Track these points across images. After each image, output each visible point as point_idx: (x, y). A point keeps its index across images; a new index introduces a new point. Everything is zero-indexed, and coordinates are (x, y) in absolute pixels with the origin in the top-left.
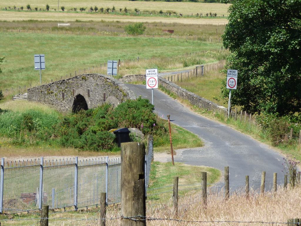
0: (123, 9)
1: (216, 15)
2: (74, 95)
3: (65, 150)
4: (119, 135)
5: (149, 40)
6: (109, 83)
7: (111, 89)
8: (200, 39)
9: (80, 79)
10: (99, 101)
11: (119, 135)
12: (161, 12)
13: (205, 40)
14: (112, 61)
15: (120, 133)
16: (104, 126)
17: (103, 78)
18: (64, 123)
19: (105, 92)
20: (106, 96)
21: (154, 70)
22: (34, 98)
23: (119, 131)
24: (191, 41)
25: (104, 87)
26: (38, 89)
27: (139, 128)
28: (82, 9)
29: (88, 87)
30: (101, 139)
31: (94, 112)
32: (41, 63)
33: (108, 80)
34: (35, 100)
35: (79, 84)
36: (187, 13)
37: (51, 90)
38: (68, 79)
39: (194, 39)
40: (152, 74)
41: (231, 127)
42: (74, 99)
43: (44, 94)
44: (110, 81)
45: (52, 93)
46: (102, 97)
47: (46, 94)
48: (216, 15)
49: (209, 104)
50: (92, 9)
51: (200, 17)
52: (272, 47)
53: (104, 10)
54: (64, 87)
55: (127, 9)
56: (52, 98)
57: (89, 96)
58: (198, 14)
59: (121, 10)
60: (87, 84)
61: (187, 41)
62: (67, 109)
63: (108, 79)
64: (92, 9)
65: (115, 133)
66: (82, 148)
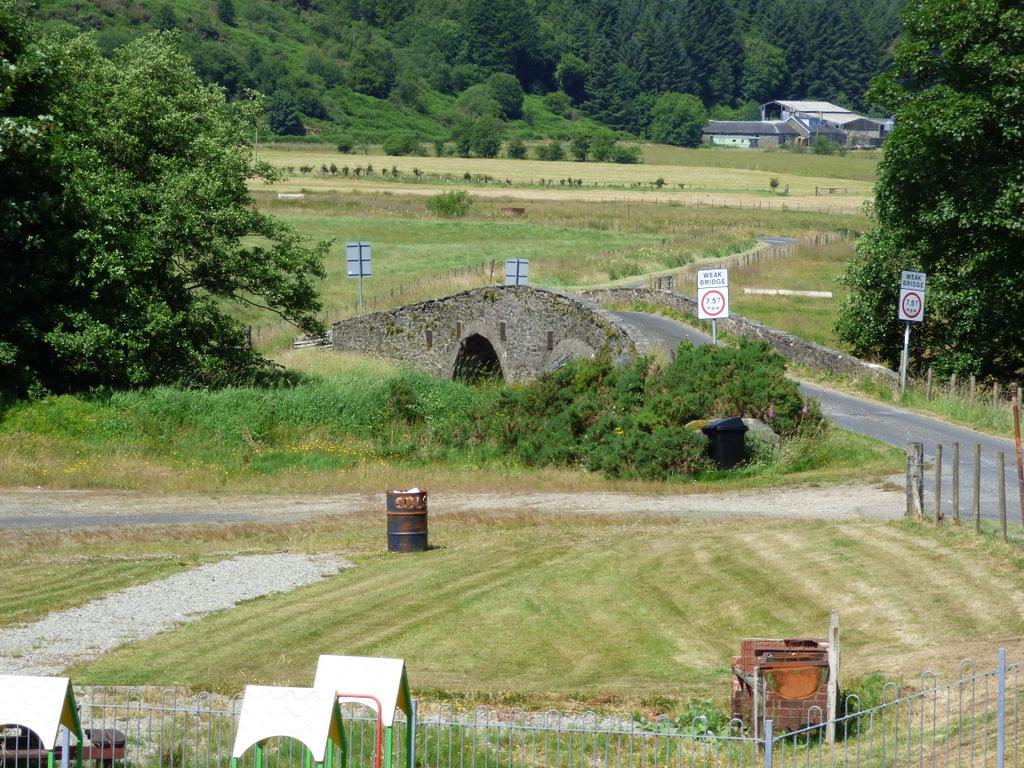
0: (390, 169)
1: (580, 182)
2: (459, 336)
3: (536, 473)
4: (719, 437)
5: (486, 227)
6: (565, 308)
7: (569, 321)
8: (592, 225)
9: (478, 297)
10: (534, 350)
11: (719, 437)
12: (467, 176)
13: (604, 228)
14: (515, 260)
15: (721, 432)
16: (670, 410)
17: (546, 295)
18: (503, 404)
19: (552, 329)
20: (556, 339)
21: (717, 271)
22: (351, 344)
23: (718, 428)
24: (577, 229)
25: (549, 316)
26: (362, 322)
27: (762, 418)
28: (305, 170)
29: (501, 318)
30: (667, 445)
31: (577, 376)
32: (361, 261)
33: (561, 300)
34: (355, 349)
35: (474, 310)
36: (520, 180)
37: (398, 325)
38: (442, 298)
39: (582, 225)
40: (714, 282)
41: (929, 415)
42: (459, 346)
43: (380, 335)
44: (566, 302)
45: (398, 331)
46: (541, 339)
47: (383, 334)
48: (580, 182)
49: (835, 357)
50: (325, 169)
51: (548, 187)
52: (1007, 217)
53: (351, 171)
54: (432, 319)
55: (398, 169)
56: (395, 342)
57: (503, 338)
58: (543, 181)
59: (384, 171)
60: (497, 311)
61: (566, 230)
62: (440, 370)
63: (560, 296)
64: (325, 169)
65: (706, 431)
66: (614, 471)
